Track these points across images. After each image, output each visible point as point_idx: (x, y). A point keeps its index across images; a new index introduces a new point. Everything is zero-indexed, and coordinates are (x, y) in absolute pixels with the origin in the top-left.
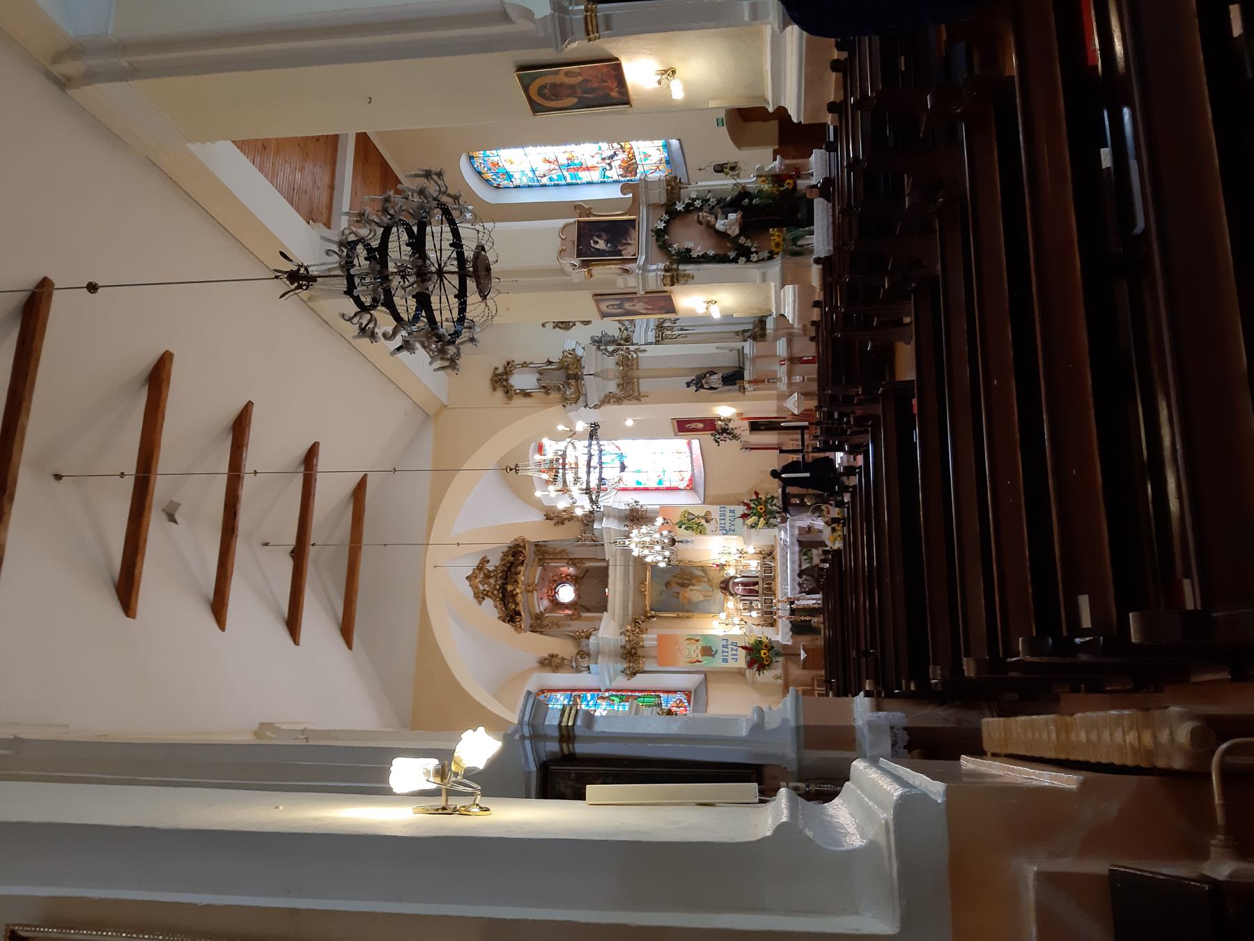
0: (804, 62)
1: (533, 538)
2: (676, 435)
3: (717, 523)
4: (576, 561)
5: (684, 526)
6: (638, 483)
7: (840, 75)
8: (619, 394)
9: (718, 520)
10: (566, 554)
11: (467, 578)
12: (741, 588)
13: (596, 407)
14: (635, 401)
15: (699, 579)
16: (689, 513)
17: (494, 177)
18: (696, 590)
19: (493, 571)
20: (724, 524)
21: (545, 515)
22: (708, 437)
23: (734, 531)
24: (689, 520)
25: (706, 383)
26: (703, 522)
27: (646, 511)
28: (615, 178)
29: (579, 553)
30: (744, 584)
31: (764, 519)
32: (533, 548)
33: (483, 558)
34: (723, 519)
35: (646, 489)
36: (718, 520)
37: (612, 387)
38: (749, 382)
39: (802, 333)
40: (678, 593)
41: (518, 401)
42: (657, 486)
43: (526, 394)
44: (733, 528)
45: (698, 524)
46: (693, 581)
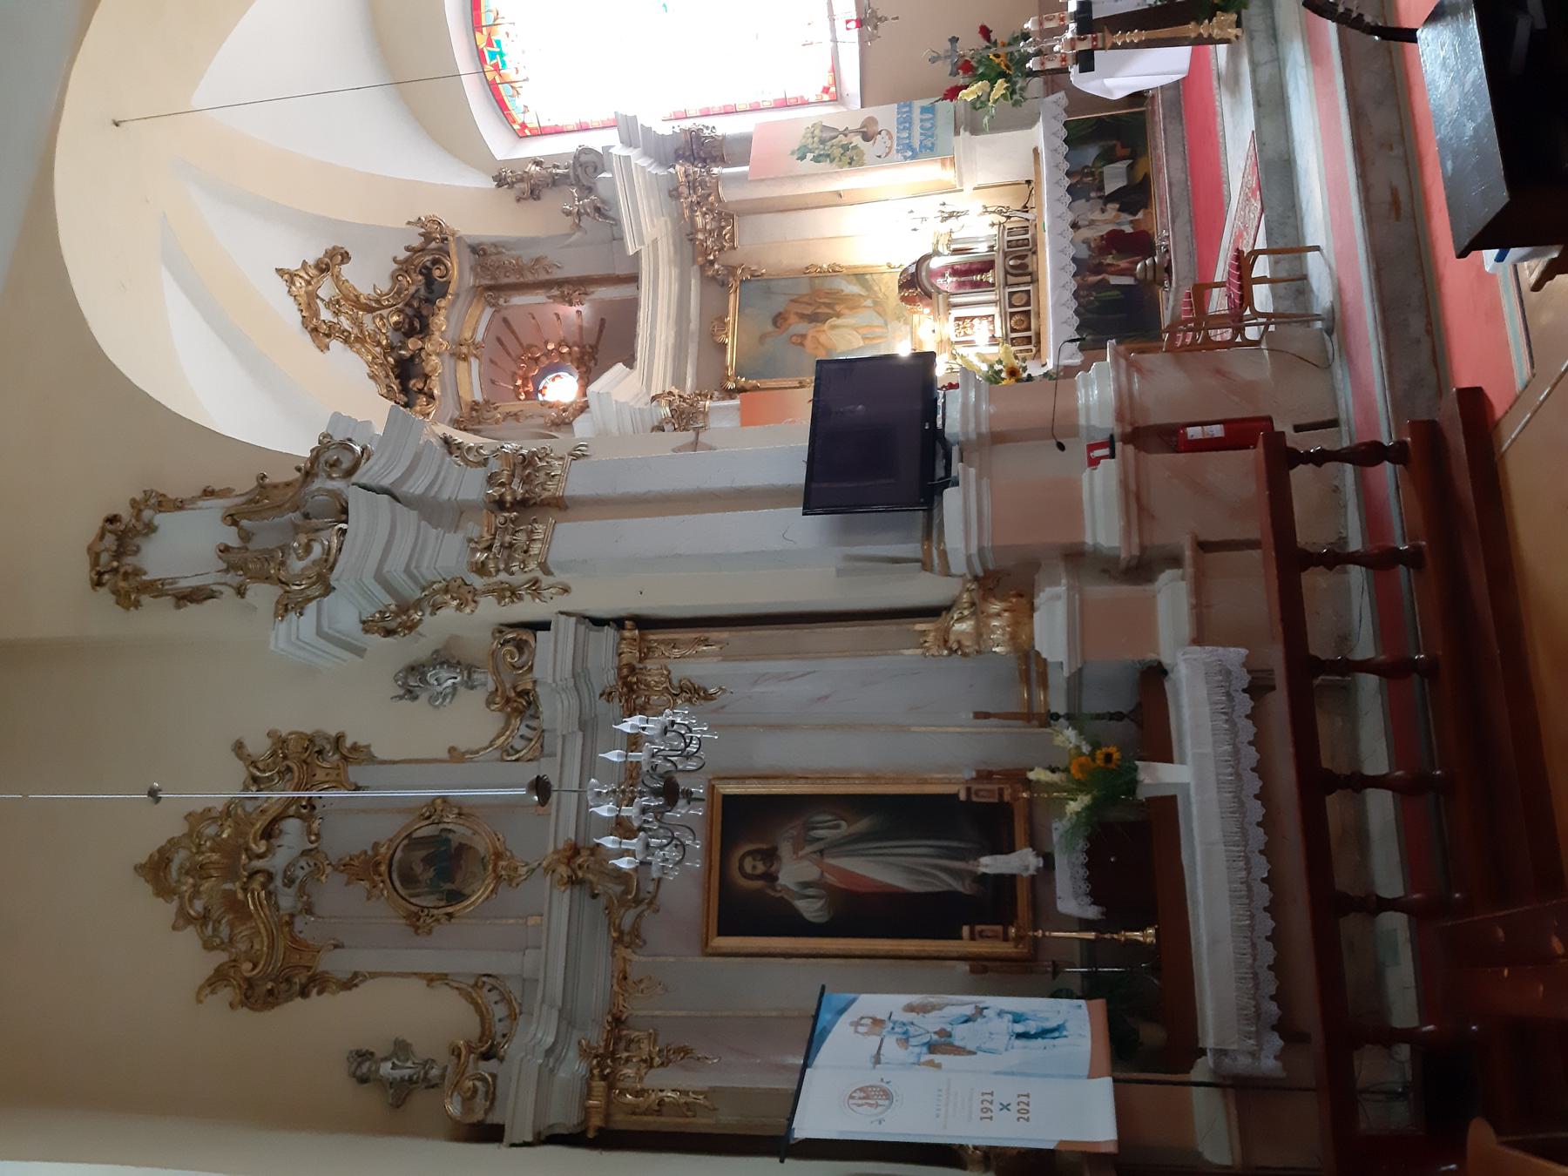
3: (891, 138)
5: (810, 156)
12: (950, 279)
15: (852, 303)
16: (825, 128)
18: (846, 326)
21: (495, 178)
23: (931, 149)
26: (857, 140)
30: (955, 272)
32: (469, 259)
34: (905, 128)
40: (804, 336)
46: (838, 308)
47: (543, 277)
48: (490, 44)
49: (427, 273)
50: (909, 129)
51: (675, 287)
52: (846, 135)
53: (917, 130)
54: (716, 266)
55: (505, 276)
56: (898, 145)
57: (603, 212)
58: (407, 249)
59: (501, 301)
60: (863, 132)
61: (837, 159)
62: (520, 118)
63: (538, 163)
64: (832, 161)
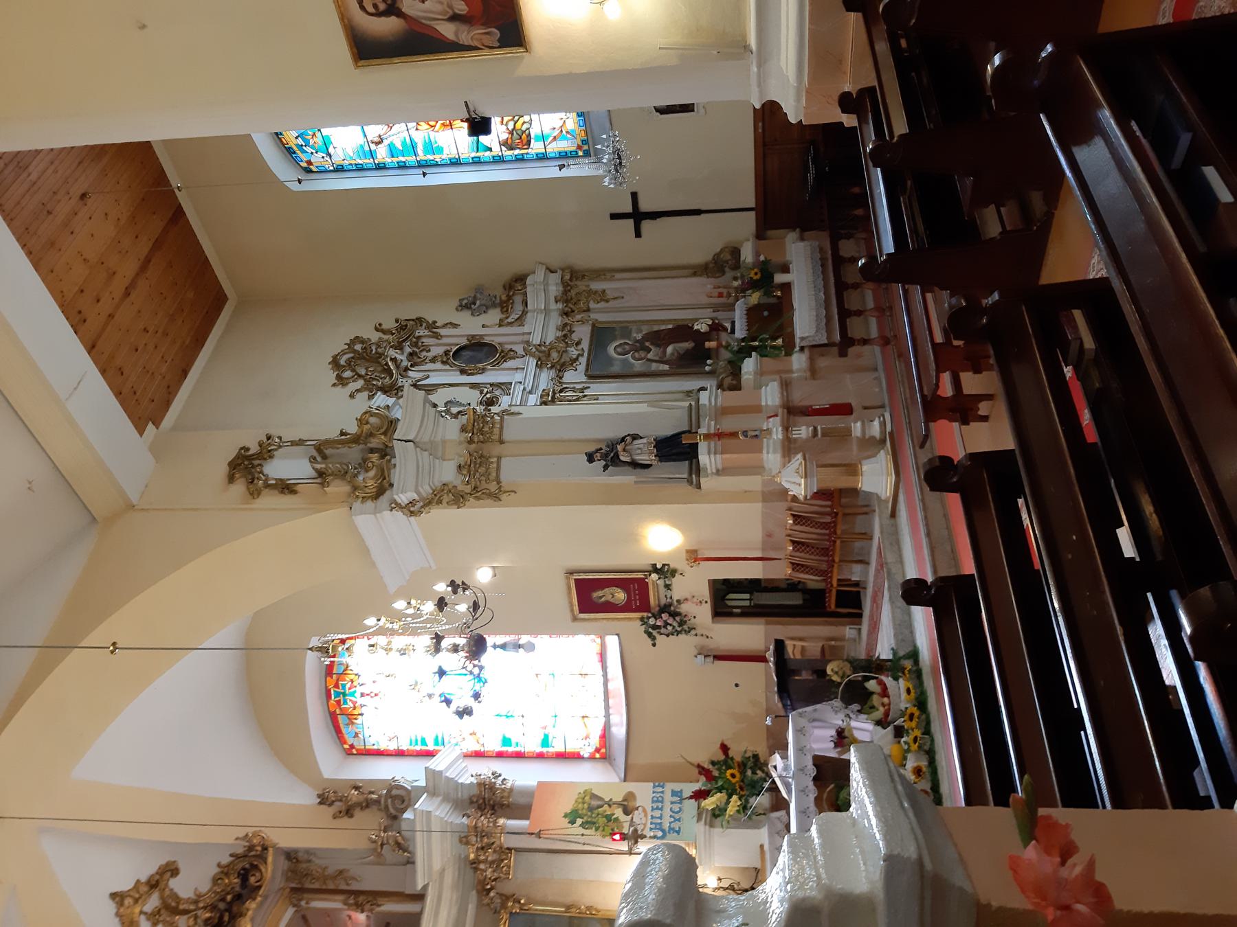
0: (807, 8)
1: (286, 840)
2: (575, 619)
3: (646, 815)
4: (361, 899)
5: (579, 821)
6: (506, 741)
7: (860, 14)
8: (460, 488)
9: (649, 810)
10: (345, 879)
11: (113, 896)
13: (411, 509)
14: (489, 501)
16: (594, 796)
17: (300, 141)
19: (188, 901)
20: (660, 818)
21: (319, 796)
22: (632, 623)
23: (678, 832)
24: (591, 809)
25: (624, 450)
26: (618, 813)
27: (511, 790)
28: (496, 150)
29: (372, 879)
31: (740, 799)
32: (284, 864)
33: (168, 864)
34: (657, 808)
35: (519, 756)
36: (649, 810)
37: (448, 473)
38: (707, 437)
39: (808, 374)
41: (270, 500)
42: (539, 749)
43: (286, 487)
44: (676, 826)
45: (609, 818)
47: (343, 887)
48: (337, 686)
49: (244, 876)
50: (661, 809)
51: (454, 911)
52: (610, 806)
53: (667, 812)
54: (492, 894)
55: (310, 882)
56: (651, 823)
57: (403, 850)
58: (231, 855)
59: (303, 903)
60: (624, 805)
61: (601, 829)
62: (350, 740)
63: (357, 788)
64: (597, 829)
